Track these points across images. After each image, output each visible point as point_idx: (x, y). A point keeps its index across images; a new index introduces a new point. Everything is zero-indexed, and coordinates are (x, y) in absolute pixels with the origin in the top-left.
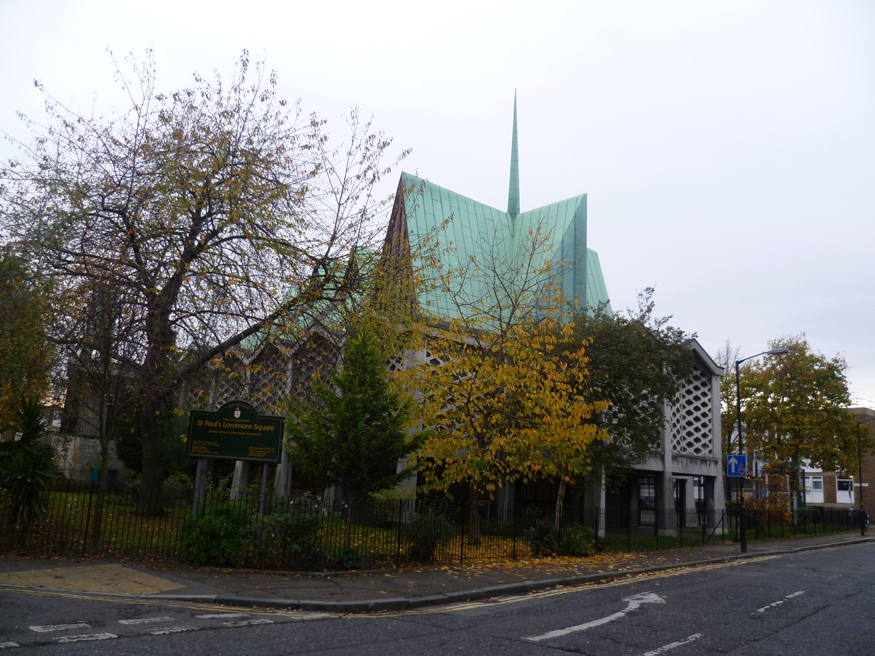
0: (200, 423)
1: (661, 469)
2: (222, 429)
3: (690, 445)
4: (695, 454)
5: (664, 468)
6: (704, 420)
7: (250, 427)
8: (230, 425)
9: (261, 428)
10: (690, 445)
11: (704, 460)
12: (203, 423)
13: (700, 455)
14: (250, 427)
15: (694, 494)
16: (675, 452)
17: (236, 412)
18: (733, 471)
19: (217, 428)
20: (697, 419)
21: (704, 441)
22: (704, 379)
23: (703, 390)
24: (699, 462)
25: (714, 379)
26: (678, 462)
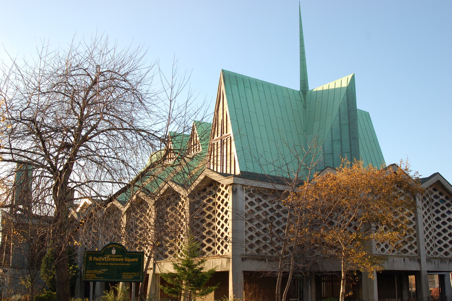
1: (419, 269)
3: (440, 250)
4: (445, 257)
5: (421, 268)
7: (122, 260)
10: (440, 250)
12: (93, 259)
13: (449, 256)
14: (122, 260)
17: (113, 251)
26: (432, 262)
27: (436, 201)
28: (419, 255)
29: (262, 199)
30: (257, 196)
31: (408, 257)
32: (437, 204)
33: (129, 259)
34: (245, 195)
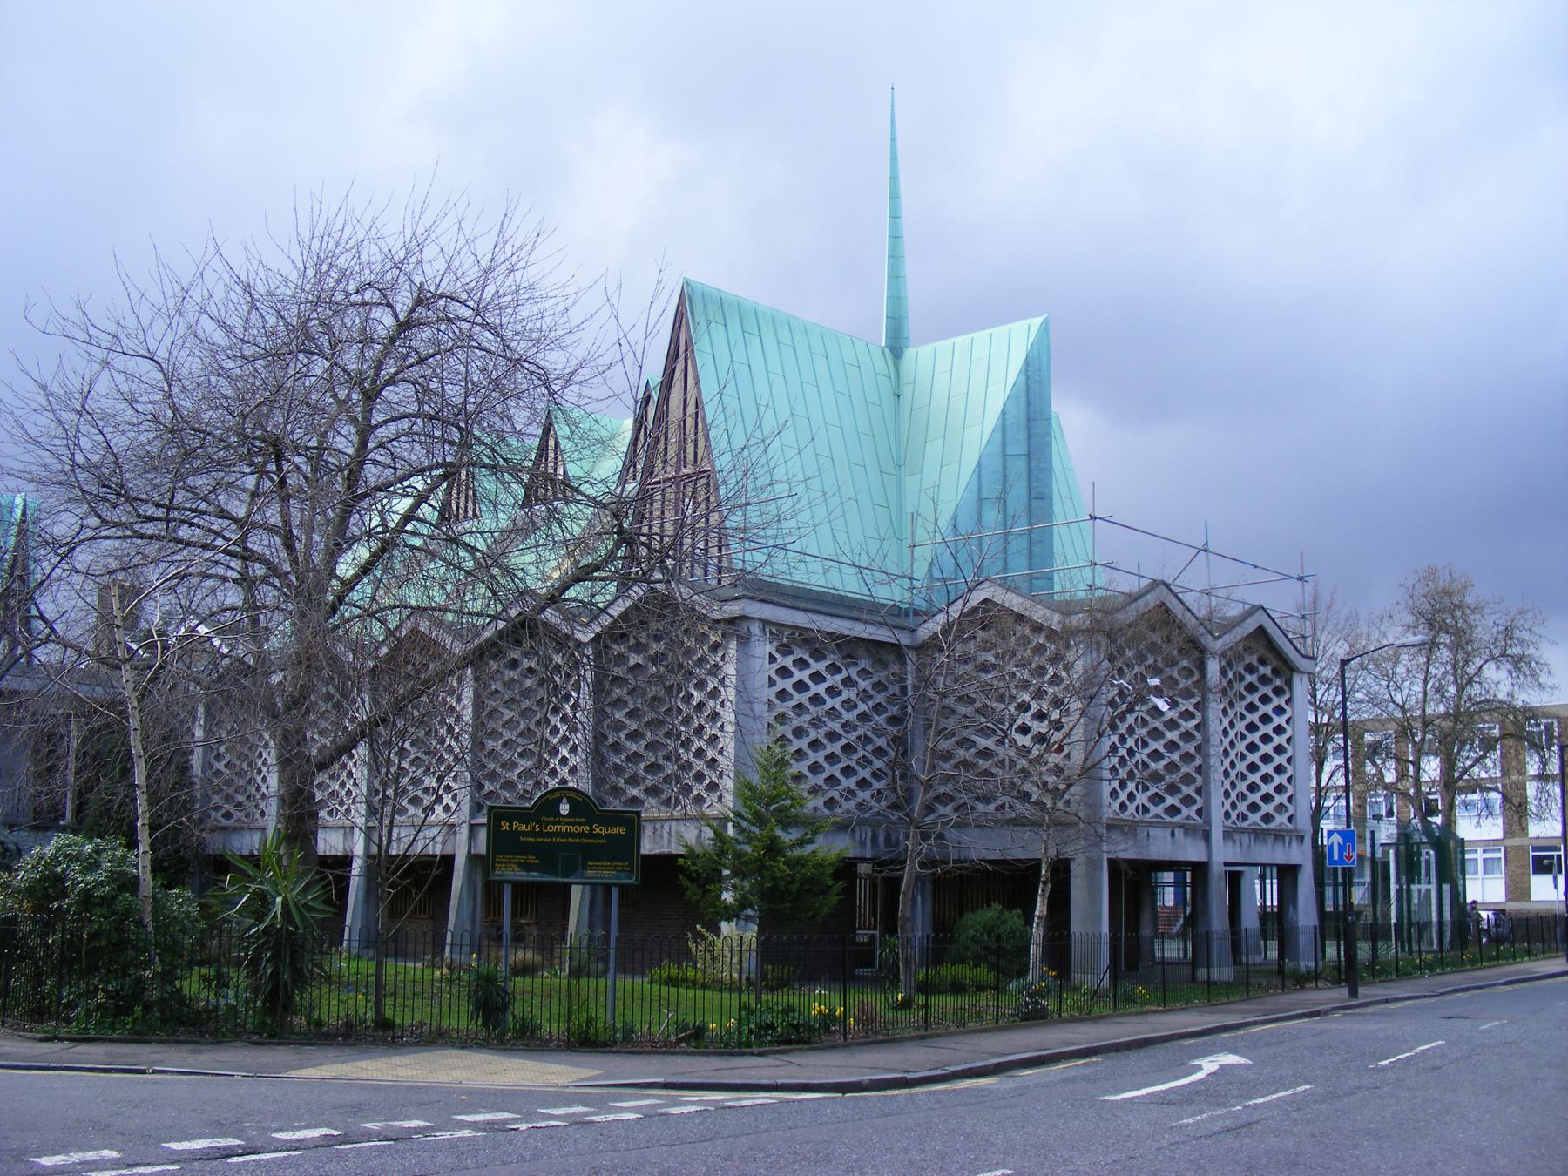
0: (505, 826)
1: (1204, 858)
2: (541, 834)
3: (1254, 807)
4: (1264, 826)
5: (1210, 855)
6: (1280, 760)
7: (586, 829)
8: (554, 828)
9: (603, 830)
10: (1254, 807)
11: (1279, 836)
12: (511, 827)
13: (1272, 826)
14: (586, 829)
15: (1262, 894)
16: (1229, 823)
17: (562, 806)
18: (1336, 857)
19: (533, 833)
20: (1266, 759)
21: (1279, 799)
22: (1278, 682)
23: (1276, 701)
24: (1270, 840)
25: (1296, 678)
26: (1234, 841)
27: (1250, 678)
28: (1208, 822)
29: (811, 661)
30: (798, 653)
31: (1182, 826)
32: (1251, 688)
33: (604, 829)
34: (770, 648)
